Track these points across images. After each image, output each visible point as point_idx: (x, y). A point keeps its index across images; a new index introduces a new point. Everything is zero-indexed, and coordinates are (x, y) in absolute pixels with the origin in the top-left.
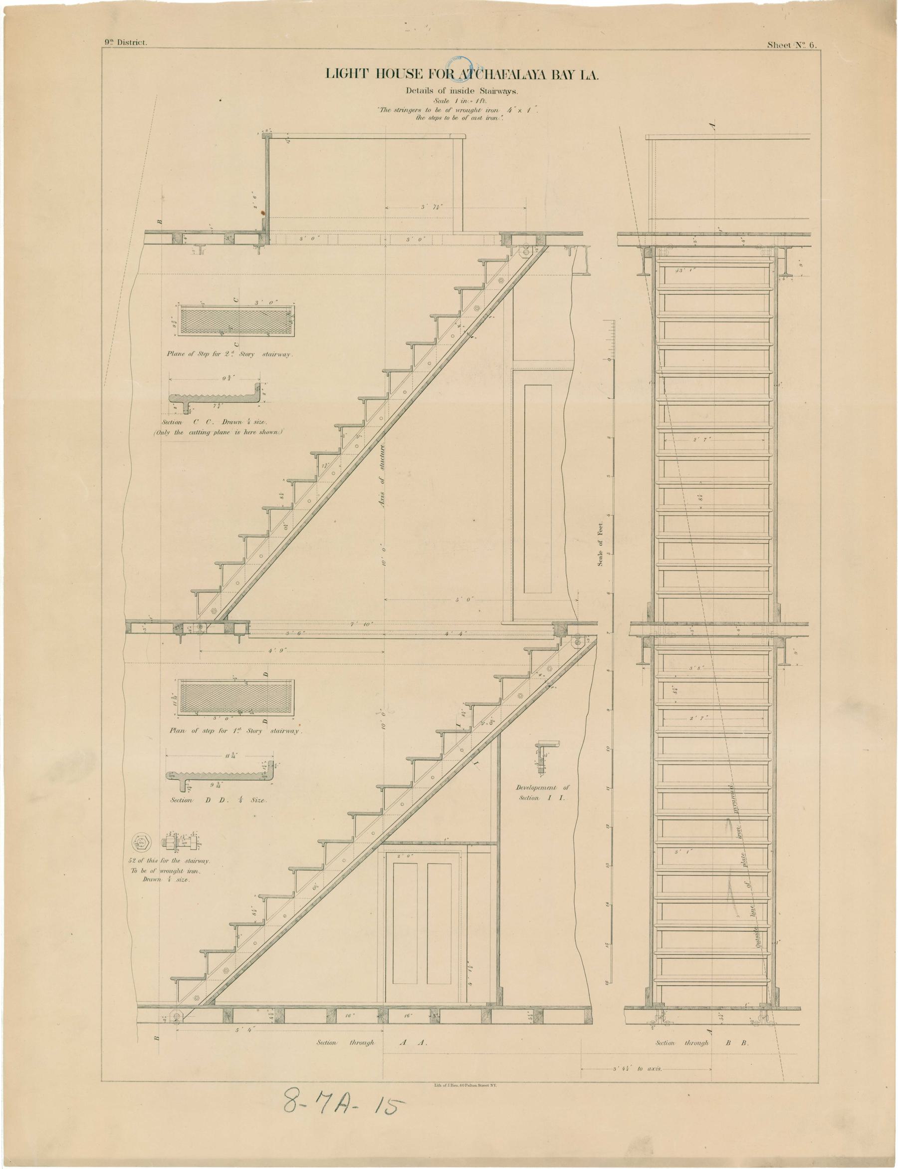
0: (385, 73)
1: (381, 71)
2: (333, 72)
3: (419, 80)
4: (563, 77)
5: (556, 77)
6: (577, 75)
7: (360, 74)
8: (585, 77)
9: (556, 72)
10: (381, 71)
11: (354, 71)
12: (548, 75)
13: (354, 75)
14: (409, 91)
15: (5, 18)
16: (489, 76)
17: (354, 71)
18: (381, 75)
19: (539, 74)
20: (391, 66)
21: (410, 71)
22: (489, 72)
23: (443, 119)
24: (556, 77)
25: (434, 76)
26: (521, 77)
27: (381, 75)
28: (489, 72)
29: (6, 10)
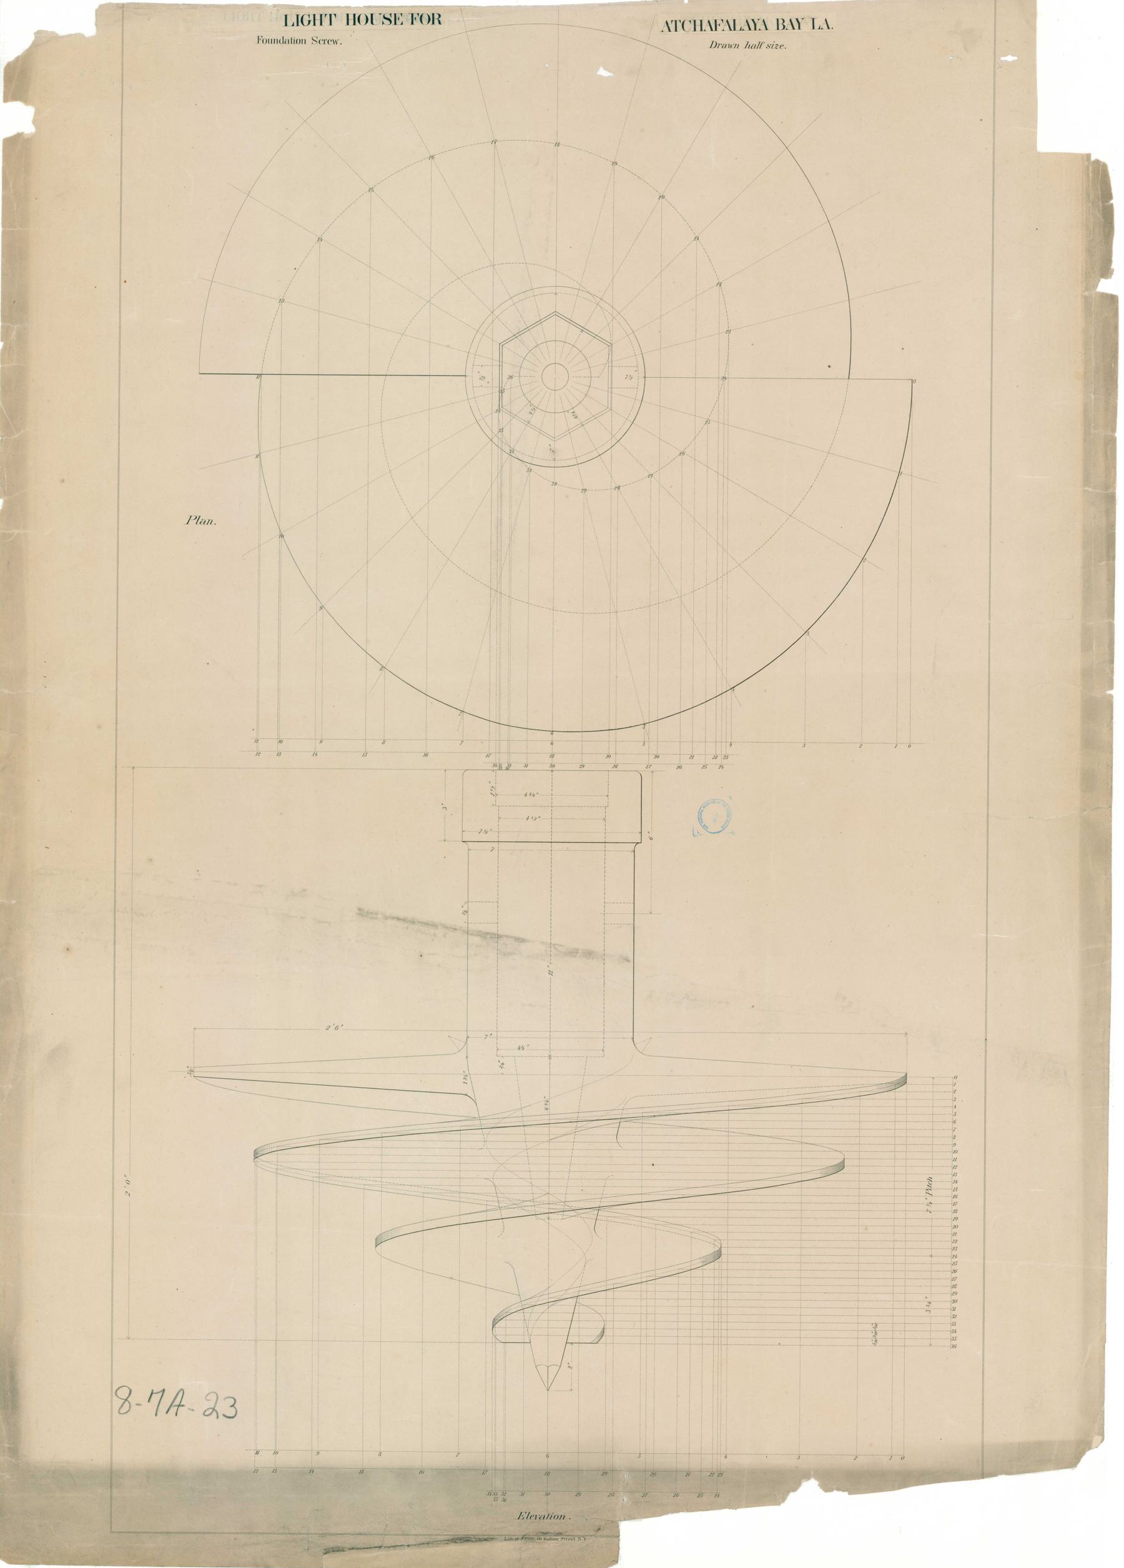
0: (357, 19)
1: (351, 17)
2: (292, 19)
3: (399, 26)
4: (790, 27)
5: (781, 27)
6: (806, 26)
7: (326, 20)
8: (816, 27)
9: (781, 22)
10: (351, 17)
11: (318, 17)
13: (318, 22)
14: (715, 45)
15: (1110, 197)
16: (698, 28)
17: (318, 17)
18: (351, 22)
19: (760, 25)
21: (387, 16)
22: (698, 23)
23: (309, 41)
24: (781, 27)
25: (417, 22)
26: (738, 28)
27: (351, 22)
28: (698, 23)
29: (5, 100)
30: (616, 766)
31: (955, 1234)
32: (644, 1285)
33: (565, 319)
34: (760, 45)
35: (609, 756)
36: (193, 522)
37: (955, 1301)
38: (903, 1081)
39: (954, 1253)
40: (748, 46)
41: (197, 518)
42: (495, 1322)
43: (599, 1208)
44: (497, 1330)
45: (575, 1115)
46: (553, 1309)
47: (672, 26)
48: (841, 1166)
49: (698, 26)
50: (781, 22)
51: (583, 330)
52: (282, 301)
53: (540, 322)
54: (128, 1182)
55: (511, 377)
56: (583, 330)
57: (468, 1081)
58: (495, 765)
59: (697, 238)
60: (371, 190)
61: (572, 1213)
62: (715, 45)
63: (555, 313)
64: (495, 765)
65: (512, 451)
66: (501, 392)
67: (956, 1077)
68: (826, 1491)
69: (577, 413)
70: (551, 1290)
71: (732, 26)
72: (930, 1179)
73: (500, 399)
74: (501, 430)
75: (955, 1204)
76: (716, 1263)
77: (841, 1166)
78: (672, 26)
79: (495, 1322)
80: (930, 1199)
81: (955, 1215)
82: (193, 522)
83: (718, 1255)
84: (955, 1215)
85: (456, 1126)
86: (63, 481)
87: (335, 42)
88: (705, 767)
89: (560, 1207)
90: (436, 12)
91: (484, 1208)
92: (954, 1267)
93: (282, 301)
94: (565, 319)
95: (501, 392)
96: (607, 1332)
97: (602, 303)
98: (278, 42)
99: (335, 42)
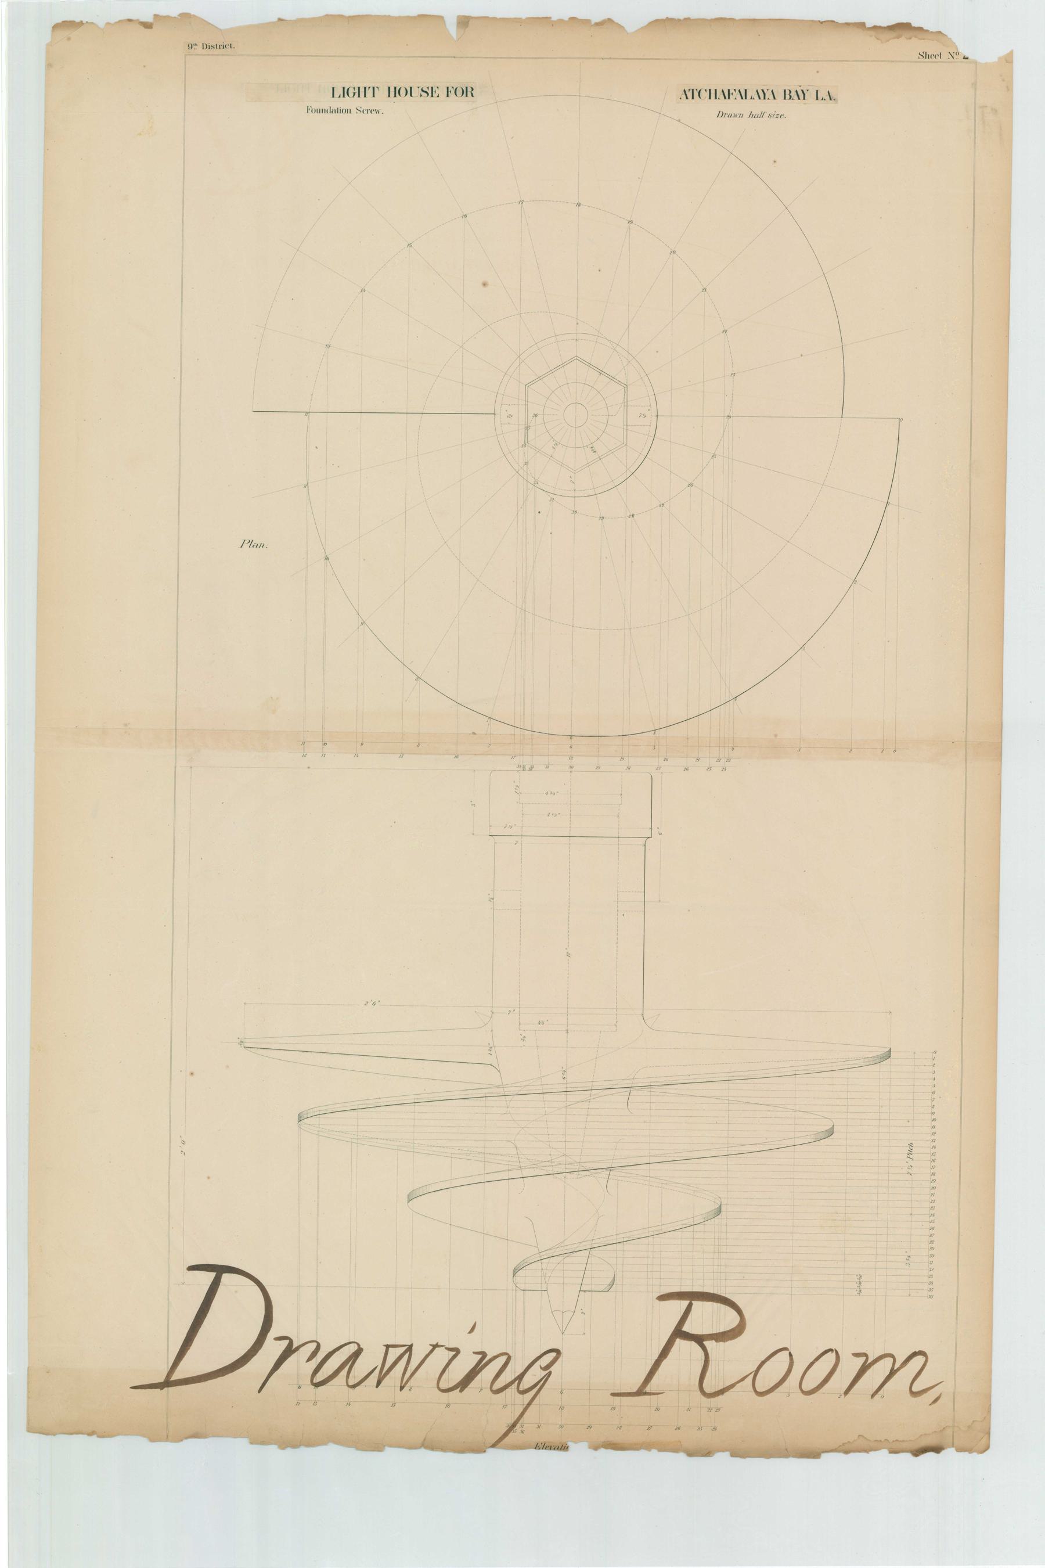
0: (397, 92)
1: (392, 90)
2: (339, 91)
4: (796, 98)
5: (788, 97)
6: (811, 96)
7: (369, 93)
8: (820, 97)
9: (787, 92)
10: (392, 90)
11: (362, 90)
12: (780, 95)
13: (362, 94)
14: (721, 114)
16: (713, 96)
17: (362, 90)
18: (392, 94)
19: (769, 95)
20: (403, 84)
21: (425, 89)
22: (713, 92)
23: (354, 111)
24: (788, 97)
25: (452, 95)
26: (748, 97)
27: (392, 94)
28: (713, 92)
30: (629, 768)
31: (933, 1195)
32: (650, 1239)
33: (583, 362)
34: (763, 114)
35: (622, 759)
36: (246, 545)
37: (932, 1256)
38: (888, 1055)
39: (932, 1211)
40: (751, 115)
41: (251, 542)
42: (515, 1271)
43: (610, 1169)
44: (518, 1279)
45: (590, 1084)
46: (567, 1260)
47: (689, 95)
48: (830, 1132)
49: (713, 94)
50: (787, 92)
51: (601, 372)
52: (328, 346)
53: (563, 365)
54: (183, 1142)
55: (536, 415)
56: (601, 372)
57: (493, 1052)
58: (519, 766)
59: (704, 290)
60: (410, 245)
61: (587, 1173)
62: (721, 114)
63: (577, 358)
64: (519, 766)
65: (536, 482)
66: (527, 428)
67: (935, 1052)
68: (283, 1449)
69: (595, 448)
70: (566, 1243)
71: (744, 95)
72: (911, 1145)
73: (526, 436)
74: (527, 463)
75: (933, 1168)
76: (716, 1219)
77: (830, 1132)
78: (689, 95)
79: (515, 1271)
80: (911, 1163)
81: (933, 1178)
82: (246, 545)
83: (719, 1211)
84: (933, 1178)
85: (482, 1093)
86: (484, 285)
87: (378, 112)
88: (709, 769)
89: (576, 1168)
90: (469, 86)
91: (506, 1167)
92: (932, 1225)
93: (328, 346)
94: (583, 362)
95: (527, 428)
96: (617, 1281)
97: (618, 349)
98: (326, 111)
99: (378, 112)
